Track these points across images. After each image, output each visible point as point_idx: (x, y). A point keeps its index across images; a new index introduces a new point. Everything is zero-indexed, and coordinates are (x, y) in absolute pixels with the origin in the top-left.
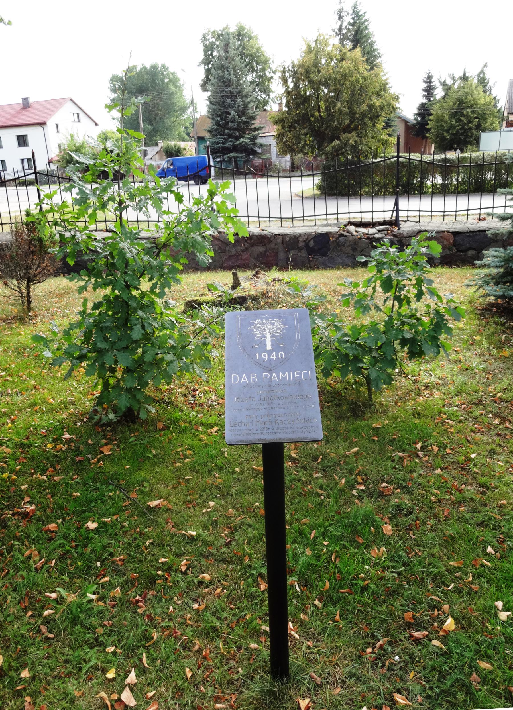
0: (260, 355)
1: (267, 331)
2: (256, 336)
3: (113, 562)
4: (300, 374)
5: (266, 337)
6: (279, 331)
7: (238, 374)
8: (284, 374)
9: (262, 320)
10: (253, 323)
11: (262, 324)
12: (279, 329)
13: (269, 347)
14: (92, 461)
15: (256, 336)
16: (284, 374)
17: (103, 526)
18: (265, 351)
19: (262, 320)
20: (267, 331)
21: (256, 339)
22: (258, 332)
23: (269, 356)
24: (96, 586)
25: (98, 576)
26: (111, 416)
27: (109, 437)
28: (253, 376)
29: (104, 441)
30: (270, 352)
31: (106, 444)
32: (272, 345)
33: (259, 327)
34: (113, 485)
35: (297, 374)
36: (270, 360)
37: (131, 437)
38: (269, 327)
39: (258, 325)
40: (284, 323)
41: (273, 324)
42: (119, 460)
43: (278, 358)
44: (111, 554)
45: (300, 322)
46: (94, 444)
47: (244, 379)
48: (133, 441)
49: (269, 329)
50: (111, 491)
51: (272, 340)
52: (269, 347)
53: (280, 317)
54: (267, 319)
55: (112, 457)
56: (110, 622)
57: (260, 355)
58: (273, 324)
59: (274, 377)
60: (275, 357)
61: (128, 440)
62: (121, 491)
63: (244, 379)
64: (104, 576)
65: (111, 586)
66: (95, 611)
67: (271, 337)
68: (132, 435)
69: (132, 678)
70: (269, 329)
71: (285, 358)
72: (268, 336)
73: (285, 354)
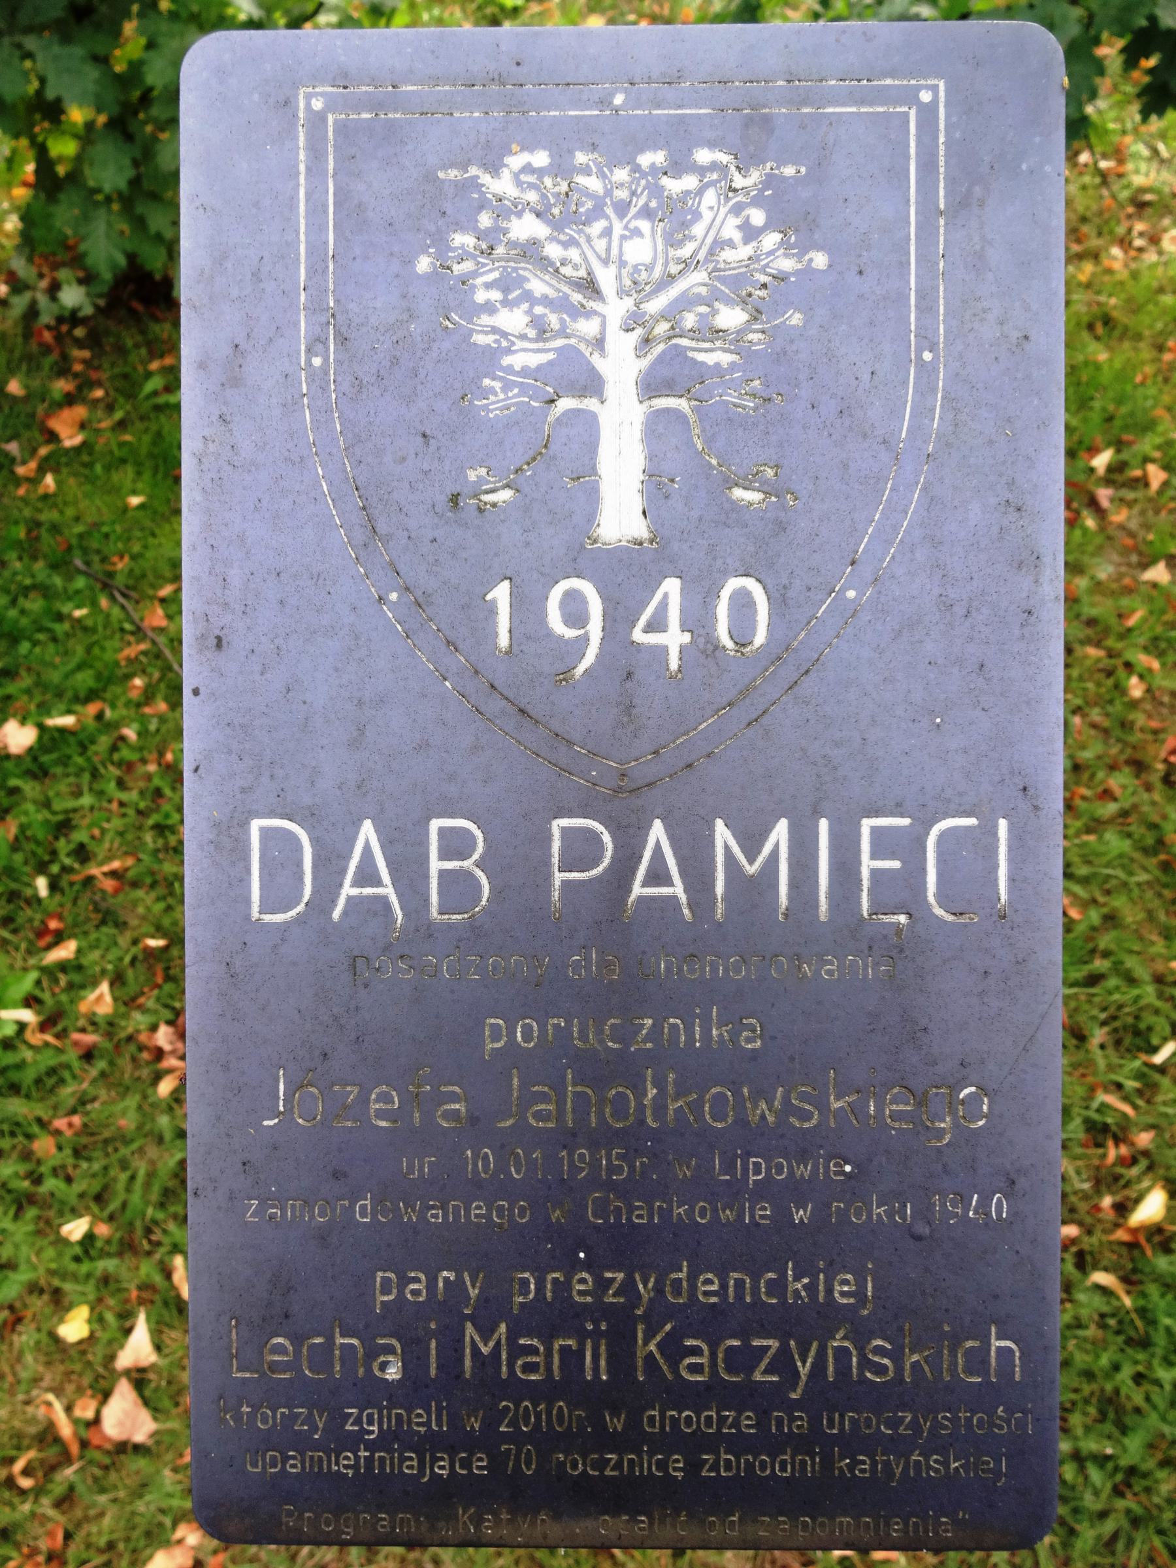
0: (527, 606)
1: (616, 309)
2: (492, 356)
3: (89, 880)
4: (908, 847)
5: (592, 385)
6: (731, 317)
7: (309, 817)
8: (752, 842)
9: (561, 168)
10: (470, 198)
11: (566, 216)
12: (736, 286)
13: (621, 518)
14: (21, 470)
15: (492, 356)
16: (752, 842)
17: (50, 740)
18: (582, 556)
19: (561, 168)
20: (616, 309)
21: (497, 400)
22: (514, 320)
23: (619, 618)
24: (33, 975)
25: (42, 932)
26: (72, 296)
27: (78, 367)
28: (454, 846)
29: (62, 386)
30: (626, 577)
31: (70, 400)
32: (656, 484)
33: (530, 251)
34: (87, 574)
35: (883, 844)
36: (625, 663)
37: (149, 375)
38: (639, 251)
39: (526, 228)
40: (795, 217)
41: (675, 217)
42: (108, 468)
43: (703, 647)
44: (82, 853)
45: (961, 205)
46: (27, 399)
47: (367, 876)
48: (155, 393)
49: (638, 287)
50: (76, 597)
51: (657, 428)
52: (621, 518)
53: (752, 135)
54: (622, 146)
55: (85, 458)
56: (77, 1120)
57: (527, 606)
58: (675, 217)
59: (658, 876)
60: (674, 639)
61: (141, 386)
62: (113, 598)
63: (367, 876)
64: (59, 938)
65: (76, 975)
66: (28, 1077)
67: (650, 387)
68: (154, 365)
69: (139, 1347)
70: (638, 287)
71: (778, 652)
72: (621, 365)
73: (779, 601)
